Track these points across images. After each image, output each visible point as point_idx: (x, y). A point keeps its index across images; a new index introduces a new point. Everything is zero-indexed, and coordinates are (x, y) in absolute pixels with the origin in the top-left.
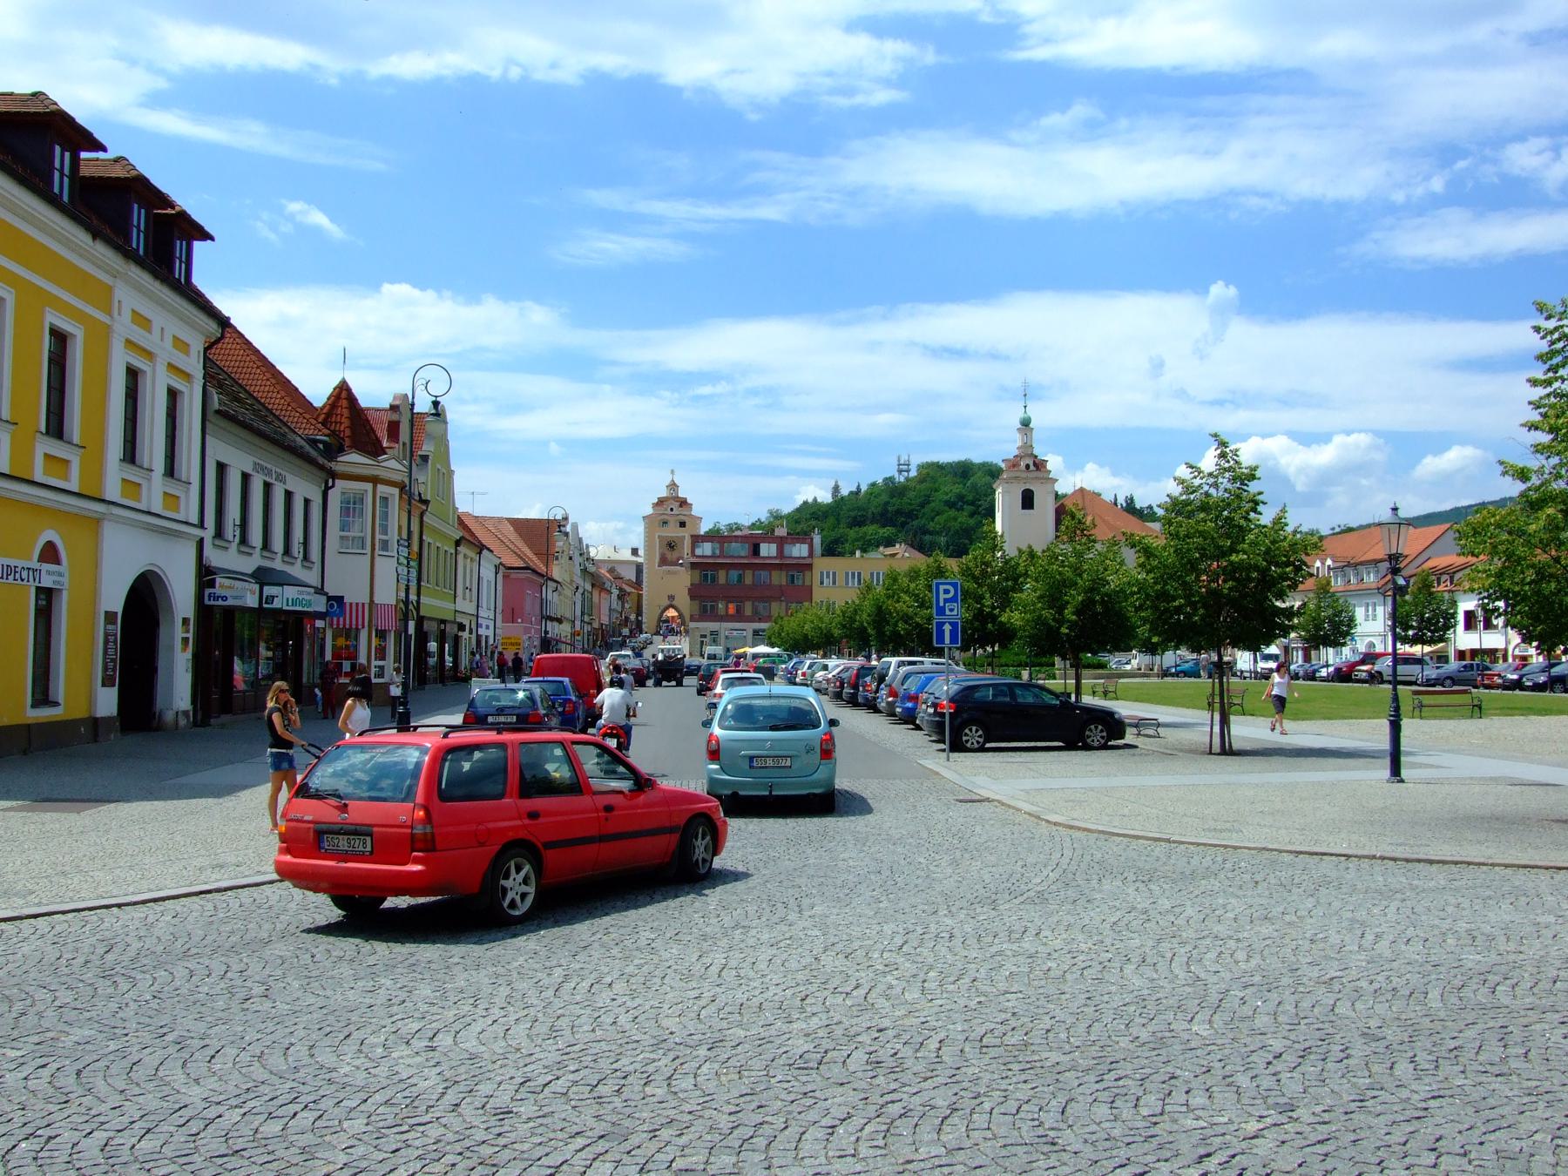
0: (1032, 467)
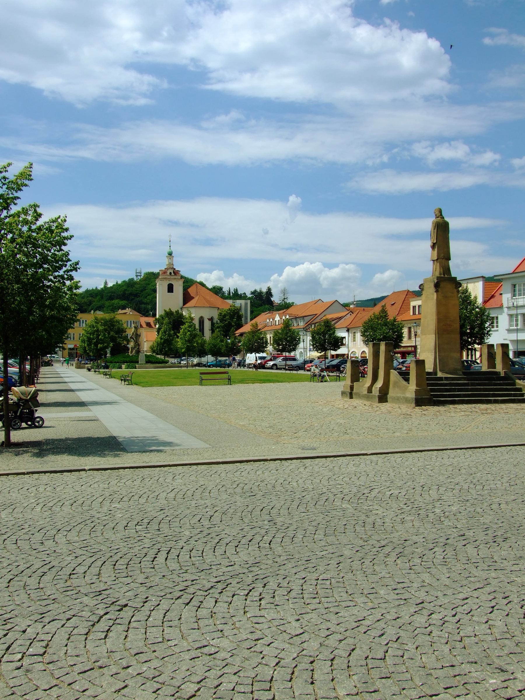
0: (173, 274)
